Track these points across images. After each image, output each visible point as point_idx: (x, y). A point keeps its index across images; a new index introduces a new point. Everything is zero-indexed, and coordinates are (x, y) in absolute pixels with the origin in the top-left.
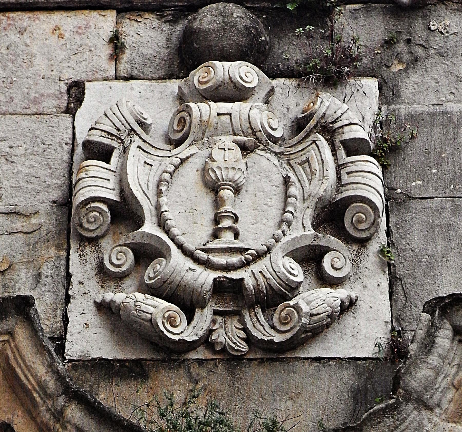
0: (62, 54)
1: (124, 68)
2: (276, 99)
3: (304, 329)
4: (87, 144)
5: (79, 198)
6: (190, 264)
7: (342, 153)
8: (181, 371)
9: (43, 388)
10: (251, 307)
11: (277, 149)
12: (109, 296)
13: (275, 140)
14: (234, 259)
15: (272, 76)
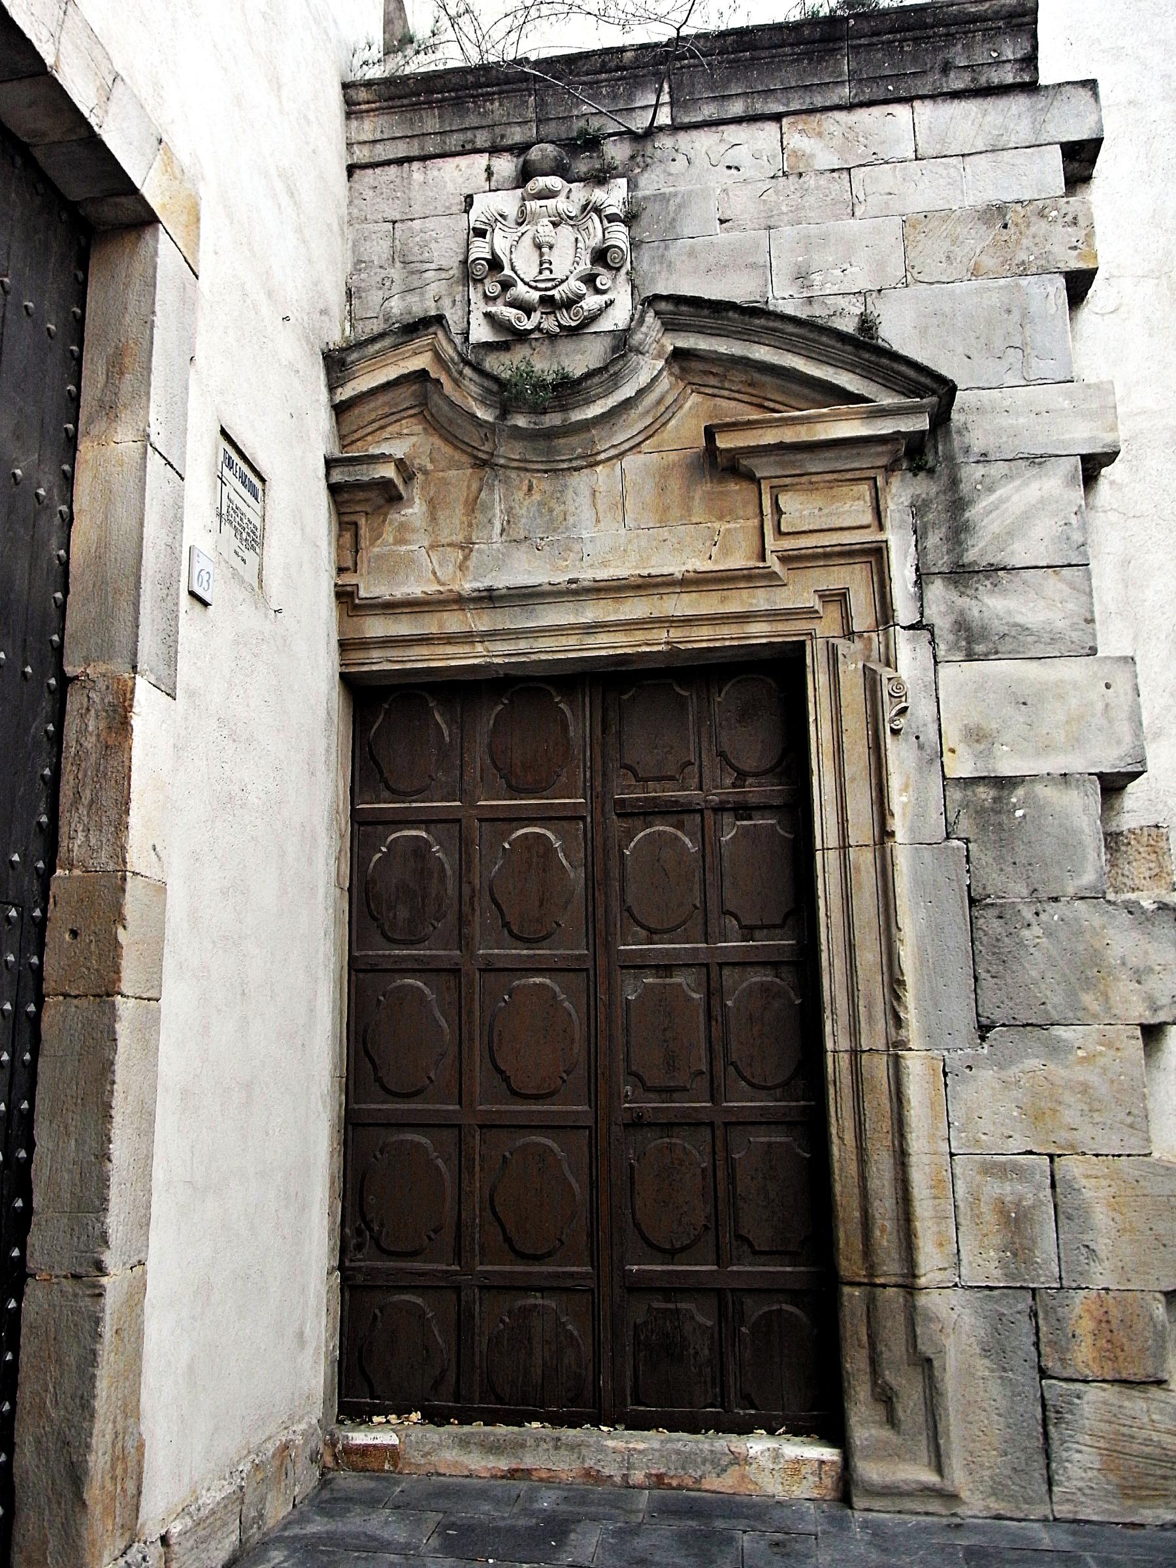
0: (461, 180)
1: (494, 185)
2: (573, 196)
3: (586, 318)
4: (474, 229)
5: (471, 259)
6: (527, 288)
7: (605, 221)
8: (527, 345)
9: (452, 359)
10: (560, 309)
11: (572, 223)
12: (489, 309)
13: (571, 218)
14: (549, 285)
15: (570, 182)
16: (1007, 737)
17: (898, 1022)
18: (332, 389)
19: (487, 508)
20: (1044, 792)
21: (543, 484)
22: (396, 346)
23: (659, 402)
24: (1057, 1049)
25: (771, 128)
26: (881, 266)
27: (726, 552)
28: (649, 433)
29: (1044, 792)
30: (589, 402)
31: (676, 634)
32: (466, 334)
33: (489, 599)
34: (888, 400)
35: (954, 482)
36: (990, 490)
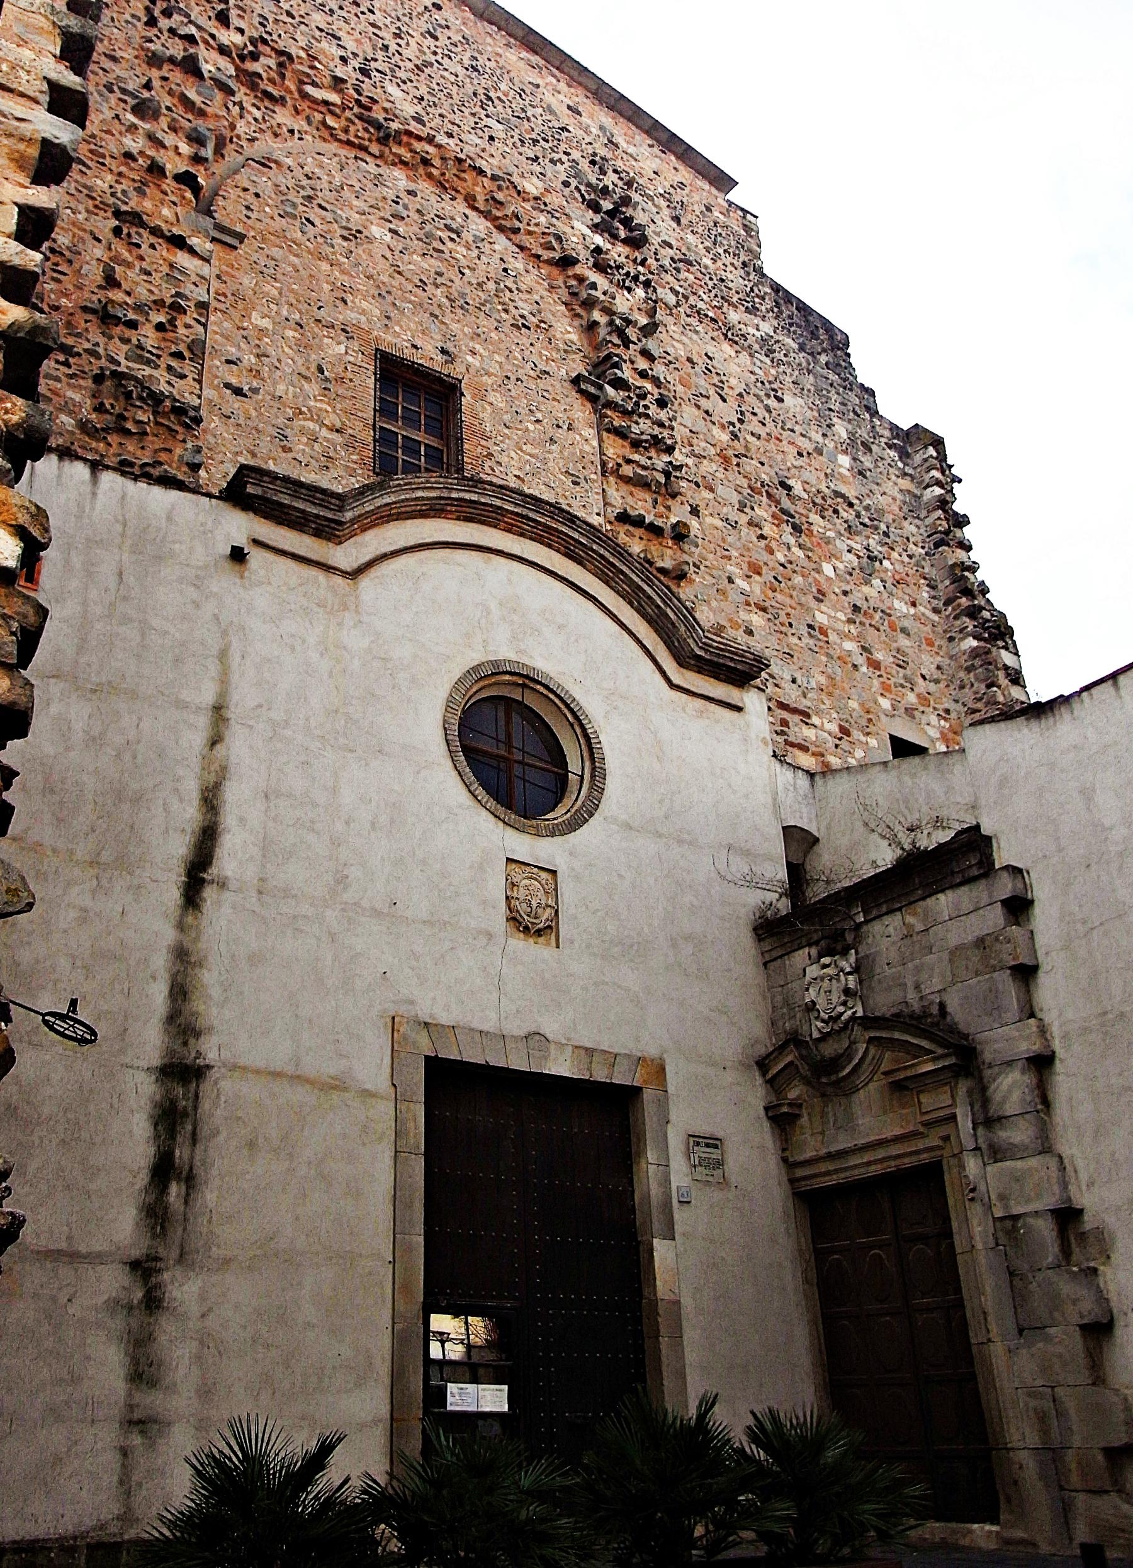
16: (1013, 1197)
17: (988, 1331)
18: (764, 1075)
19: (827, 1113)
20: (1031, 1220)
21: (844, 1101)
22: (780, 1054)
23: (873, 1058)
24: (1048, 1339)
25: (898, 913)
26: (943, 976)
27: (908, 1123)
28: (874, 1072)
29: (1031, 1220)
30: (844, 1068)
31: (897, 1162)
32: (811, 1035)
33: (830, 1157)
34: (940, 1051)
35: (981, 1078)
36: (994, 1080)
